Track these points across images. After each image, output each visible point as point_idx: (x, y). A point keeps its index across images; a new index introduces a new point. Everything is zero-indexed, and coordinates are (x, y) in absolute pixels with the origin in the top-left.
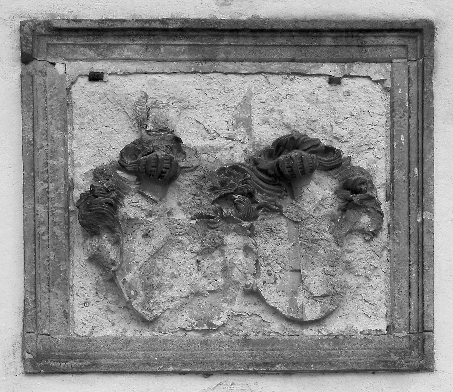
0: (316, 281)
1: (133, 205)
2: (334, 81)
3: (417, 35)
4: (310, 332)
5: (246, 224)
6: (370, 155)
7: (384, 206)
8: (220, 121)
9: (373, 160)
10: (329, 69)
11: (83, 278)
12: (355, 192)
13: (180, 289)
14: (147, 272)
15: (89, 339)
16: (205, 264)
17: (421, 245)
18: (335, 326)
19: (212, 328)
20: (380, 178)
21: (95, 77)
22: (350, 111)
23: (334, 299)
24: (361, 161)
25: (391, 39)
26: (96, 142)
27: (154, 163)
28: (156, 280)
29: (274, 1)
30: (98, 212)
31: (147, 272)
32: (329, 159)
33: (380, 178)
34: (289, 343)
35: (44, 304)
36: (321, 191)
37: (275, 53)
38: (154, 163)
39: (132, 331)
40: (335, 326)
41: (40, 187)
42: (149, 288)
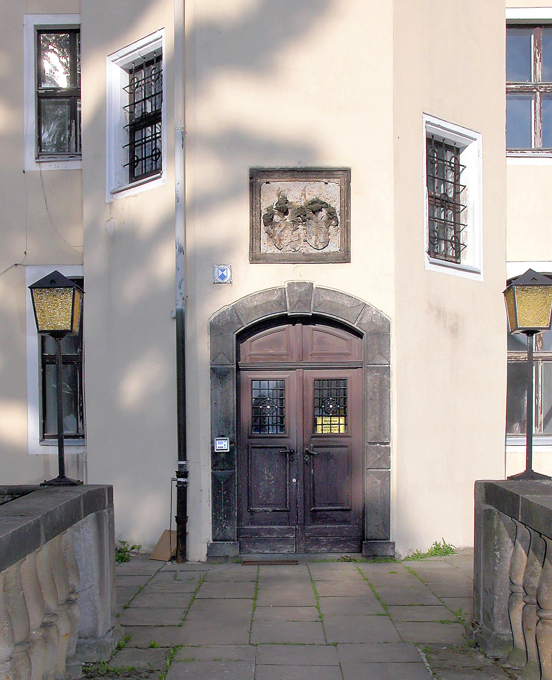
0: (321, 238)
1: (276, 218)
2: (326, 183)
3: (347, 172)
4: (320, 251)
5: (304, 223)
6: (335, 203)
7: (339, 217)
8: (298, 194)
9: (336, 205)
10: (324, 180)
11: (264, 236)
12: (331, 215)
14: (279, 236)
15: (265, 254)
16: (294, 233)
17: (347, 228)
18: (326, 250)
19: (296, 251)
20: (338, 209)
21: (267, 183)
22: (330, 192)
23: (326, 244)
24: (333, 205)
25: (340, 173)
26: (269, 200)
27: (283, 209)
28: (282, 238)
29: (24, 172)
30: (269, 221)
31: (279, 236)
32: (327, 206)
33: (338, 209)
34: (315, 254)
35: (254, 245)
37: (311, 176)
38: (283, 209)
39: (277, 251)
40: (326, 250)
41: (254, 213)
42: (280, 240)
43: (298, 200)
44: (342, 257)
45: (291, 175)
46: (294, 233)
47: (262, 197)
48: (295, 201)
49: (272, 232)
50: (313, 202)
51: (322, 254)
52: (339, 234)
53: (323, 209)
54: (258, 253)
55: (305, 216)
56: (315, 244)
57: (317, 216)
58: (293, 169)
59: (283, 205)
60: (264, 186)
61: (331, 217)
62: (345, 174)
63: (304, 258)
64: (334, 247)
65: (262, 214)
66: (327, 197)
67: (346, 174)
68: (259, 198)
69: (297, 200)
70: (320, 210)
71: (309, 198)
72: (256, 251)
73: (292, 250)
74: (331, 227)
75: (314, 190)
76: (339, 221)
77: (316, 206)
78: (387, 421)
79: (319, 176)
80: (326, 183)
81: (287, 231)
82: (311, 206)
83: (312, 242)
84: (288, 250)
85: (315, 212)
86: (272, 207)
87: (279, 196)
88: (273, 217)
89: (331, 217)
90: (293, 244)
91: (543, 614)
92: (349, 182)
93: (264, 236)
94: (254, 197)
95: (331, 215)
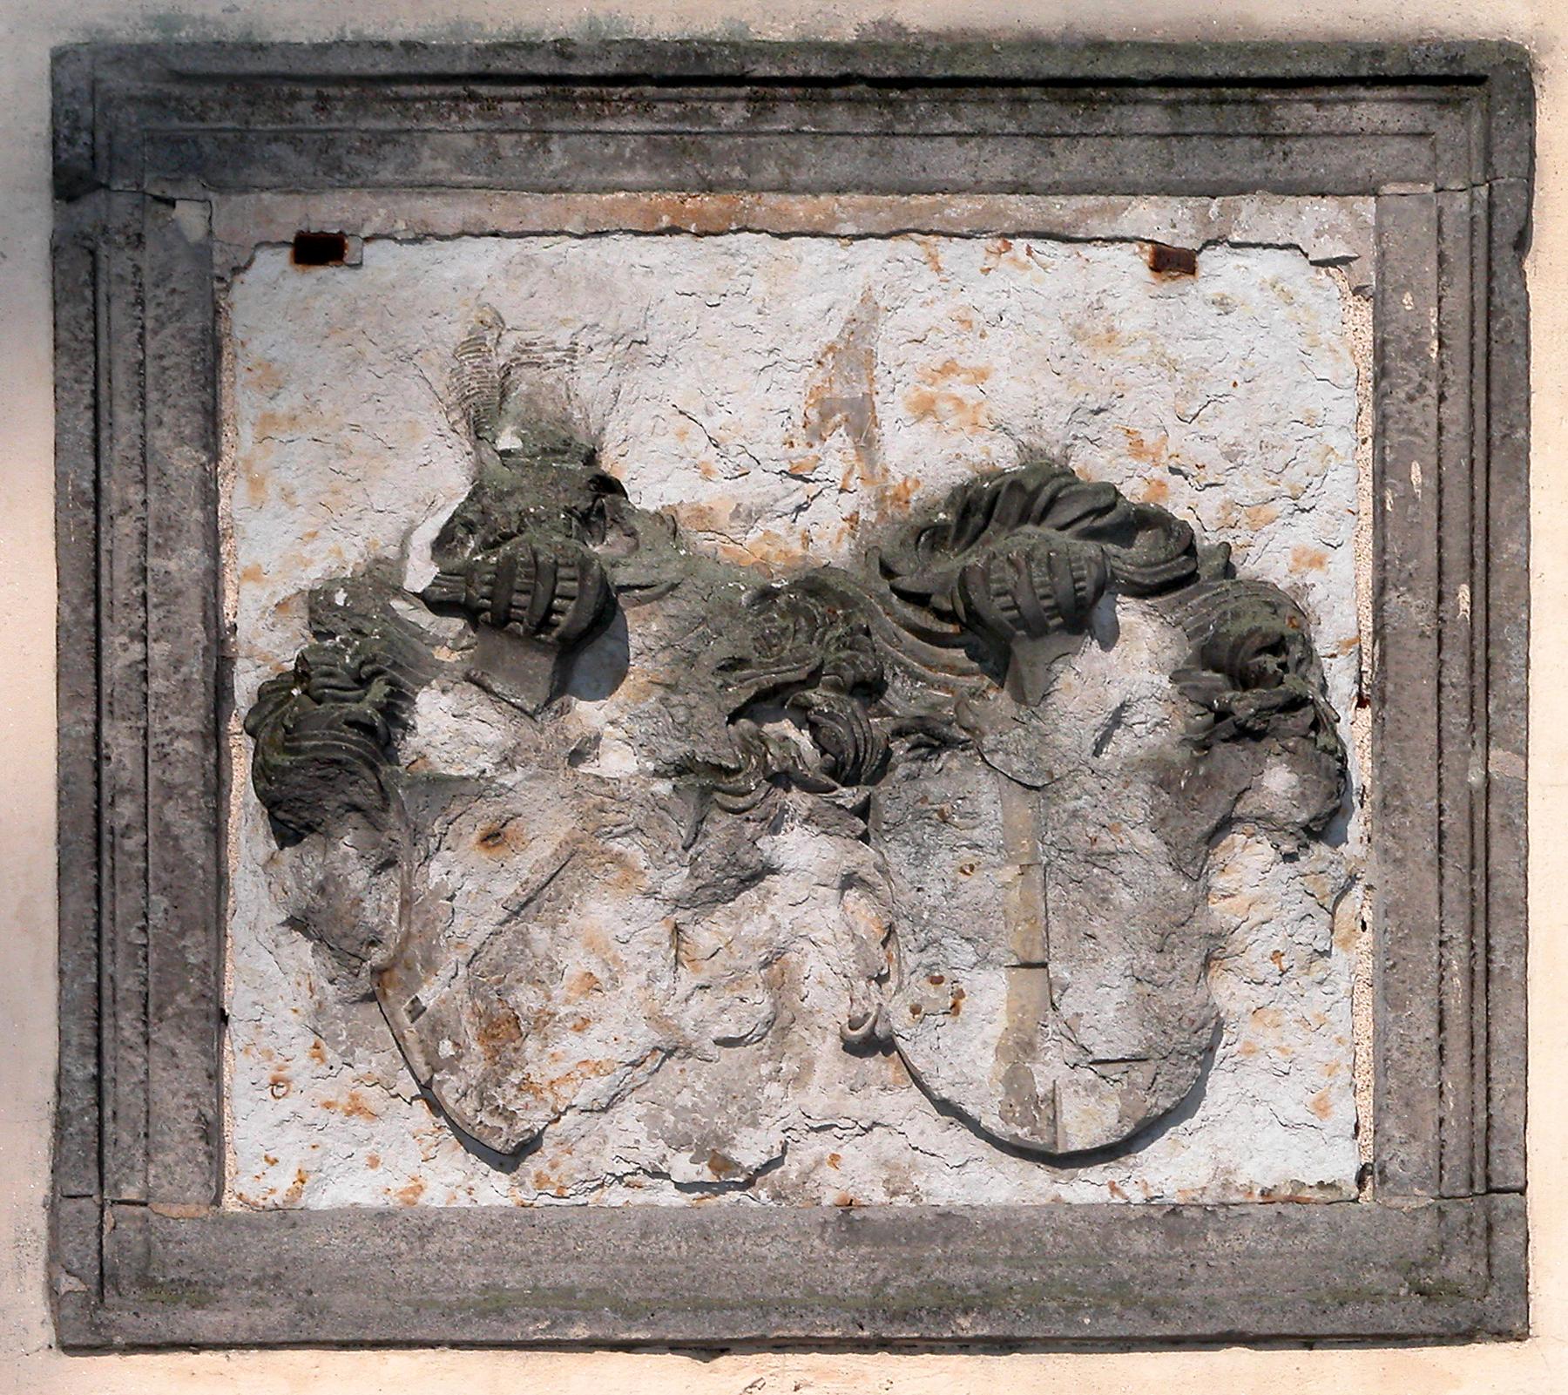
0: (1103, 1003)
1: (448, 726)
2: (1171, 262)
3: (1473, 85)
5: (849, 796)
6: (1304, 533)
7: (1356, 730)
8: (761, 405)
9: (1320, 556)
10: (1156, 218)
12: (1251, 679)
13: (613, 1034)
14: (492, 976)
15: (287, 1216)
16: (704, 937)
18: (1171, 1169)
19: (726, 1174)
21: (319, 250)
23: (1173, 1077)
24: (1269, 559)
26: (331, 495)
27: (544, 579)
28: (527, 999)
30: (332, 748)
31: (492, 976)
32: (1179, 567)
33: (1339, 610)
34: (1003, 1226)
35: (124, 1091)
36: (1132, 668)
37: (951, 160)
38: (544, 579)
39: (454, 1182)
40: (1171, 1169)
43: (762, 486)
44: (1408, 1267)
45: (669, 149)
46: (704, 937)
47: (240, 440)
48: (716, 494)
49: (378, 903)
50: (979, 509)
51: (1114, 1221)
52: (1355, 961)
53: (1128, 612)
54: (181, 1205)
55: (870, 689)
56: (1016, 1081)
57: (1031, 695)
58: (685, 49)
59: (549, 543)
60: (271, 305)
61: (1245, 705)
62: (1447, 126)
63: (850, 1271)
64: (1286, 1117)
65: (246, 682)
66: (1184, 443)
67: (1457, 129)
68: (184, 460)
69: (752, 490)
70: (1080, 618)
71: (930, 458)
72: (161, 1179)
73: (684, 1167)
74: (1248, 862)
75: (996, 351)
76: (1361, 770)
77: (1012, 568)
78: (847, 209)
79: (1075, 160)
80: (1171, 262)
81: (601, 912)
82: (949, 564)
83: (967, 1055)
84: (614, 1162)
85: (1006, 639)
86: (381, 578)
87: (479, 429)
88: (395, 711)
89: (1245, 705)
90: (688, 1086)
91: (142, 988)
92: (1502, 238)
93: (269, 977)
94: (122, 444)
95: (1243, 680)
